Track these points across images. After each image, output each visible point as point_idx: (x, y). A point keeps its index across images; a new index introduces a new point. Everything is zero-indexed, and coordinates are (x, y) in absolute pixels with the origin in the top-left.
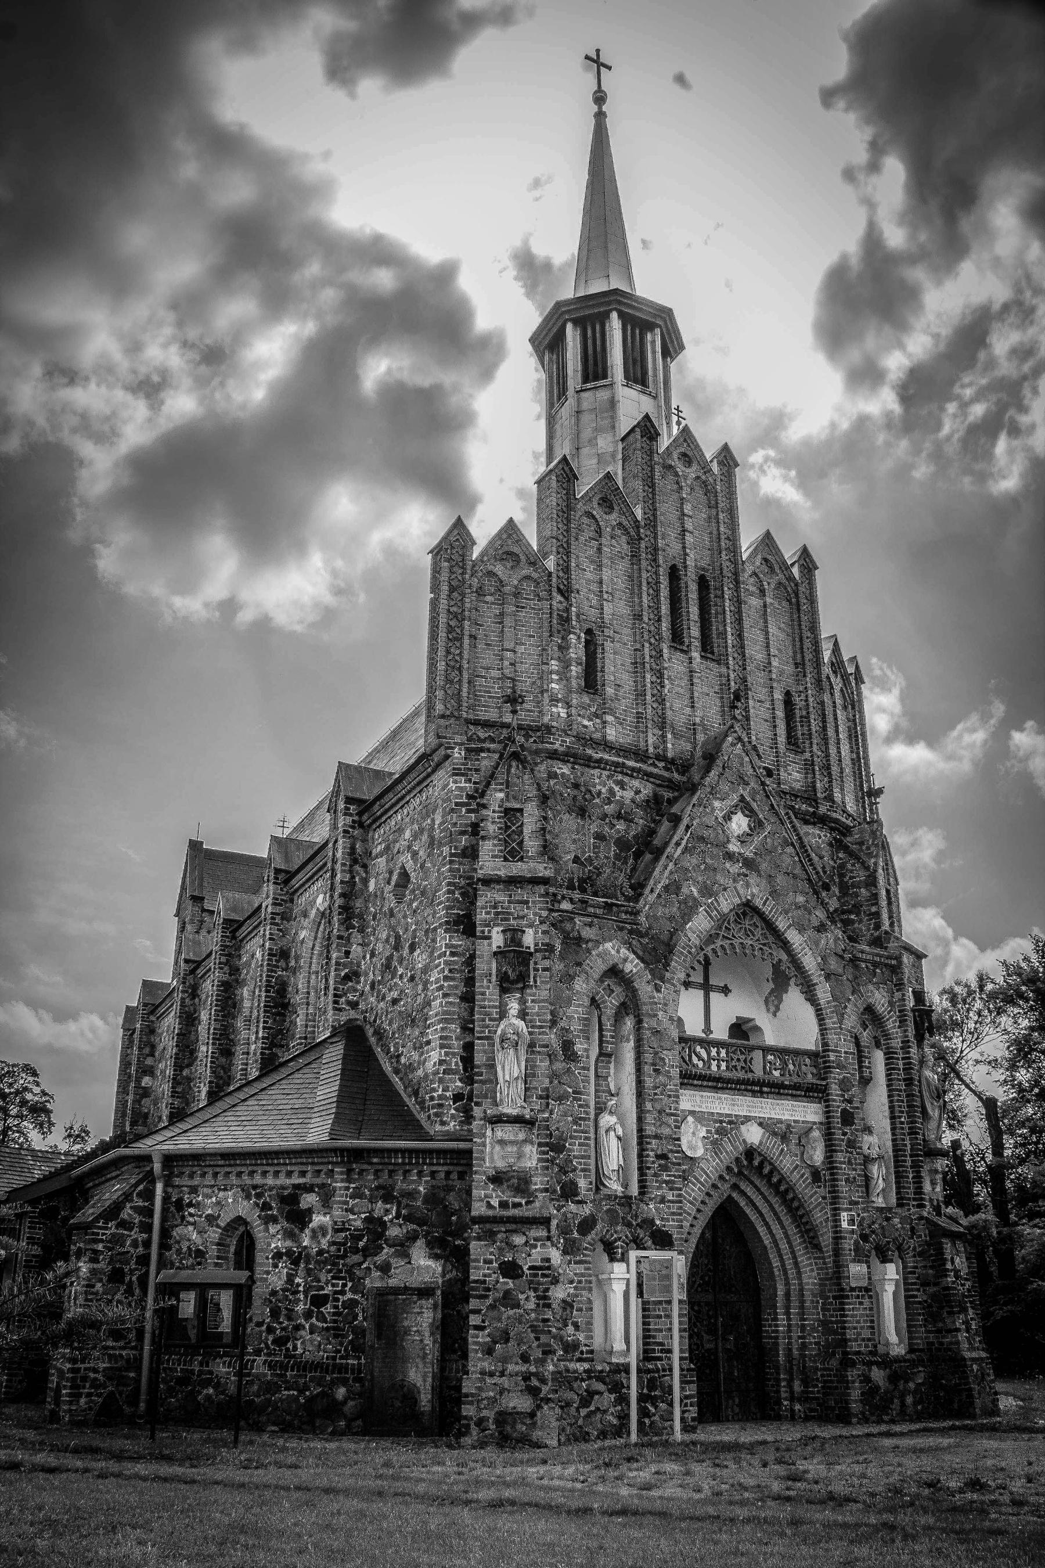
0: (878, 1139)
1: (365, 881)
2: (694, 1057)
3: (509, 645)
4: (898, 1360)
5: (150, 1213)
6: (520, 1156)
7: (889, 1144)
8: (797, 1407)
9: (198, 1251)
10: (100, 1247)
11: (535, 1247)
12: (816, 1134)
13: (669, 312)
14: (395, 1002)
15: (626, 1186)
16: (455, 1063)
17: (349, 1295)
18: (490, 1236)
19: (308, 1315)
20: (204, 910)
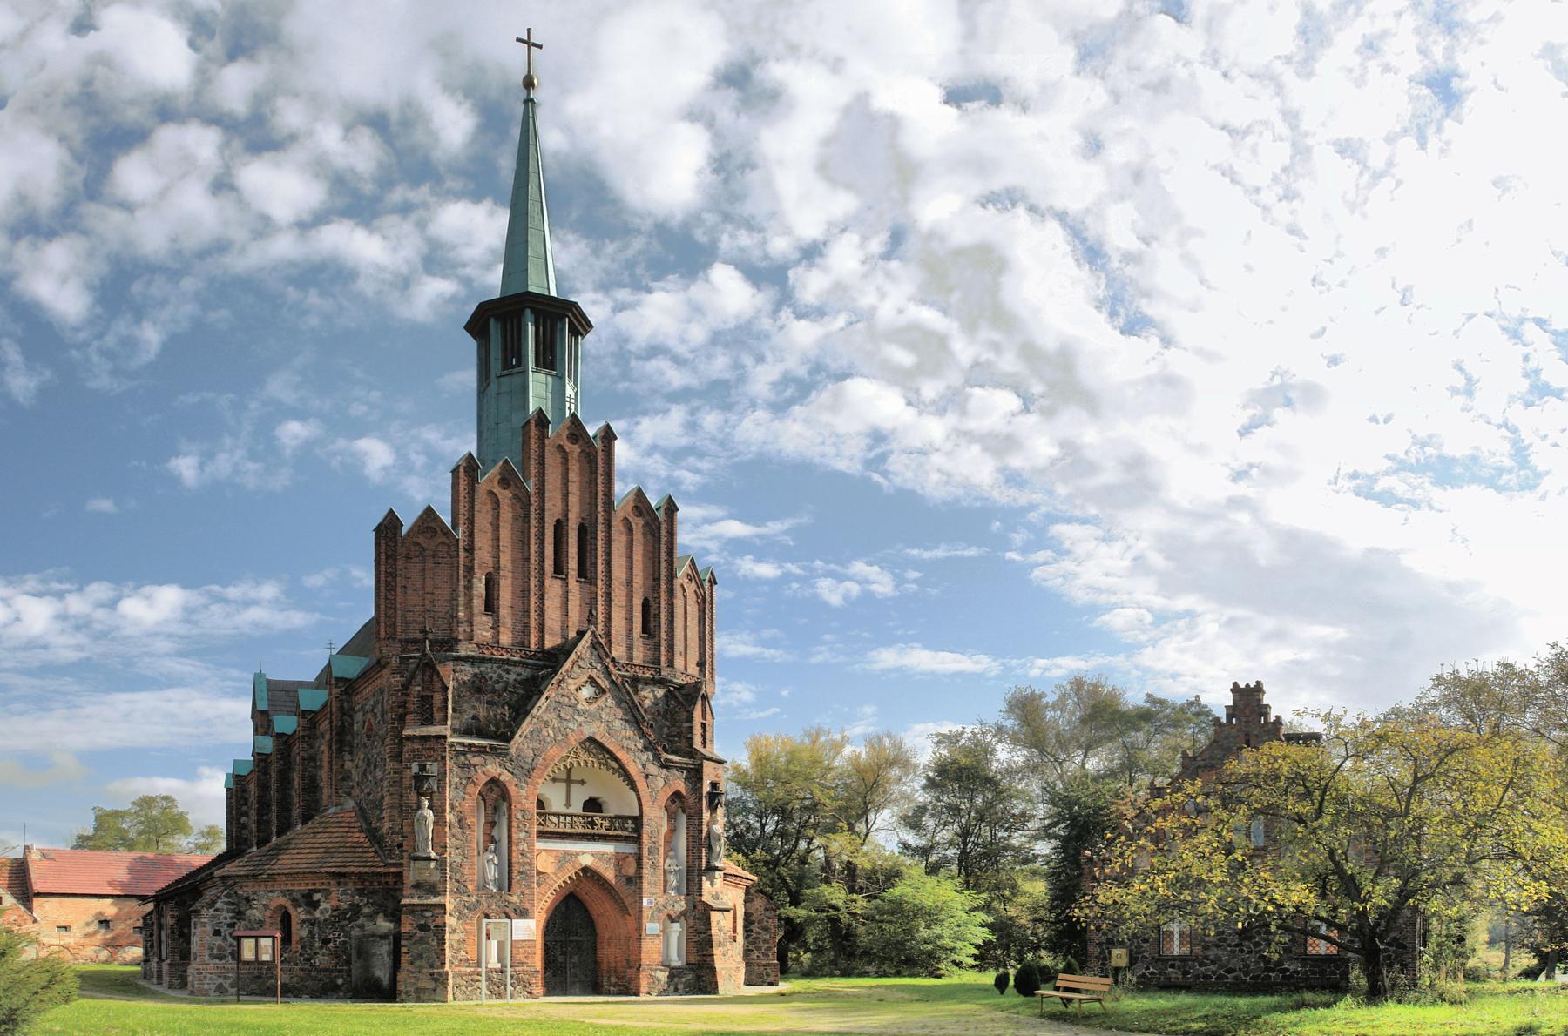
13: (378, 530)
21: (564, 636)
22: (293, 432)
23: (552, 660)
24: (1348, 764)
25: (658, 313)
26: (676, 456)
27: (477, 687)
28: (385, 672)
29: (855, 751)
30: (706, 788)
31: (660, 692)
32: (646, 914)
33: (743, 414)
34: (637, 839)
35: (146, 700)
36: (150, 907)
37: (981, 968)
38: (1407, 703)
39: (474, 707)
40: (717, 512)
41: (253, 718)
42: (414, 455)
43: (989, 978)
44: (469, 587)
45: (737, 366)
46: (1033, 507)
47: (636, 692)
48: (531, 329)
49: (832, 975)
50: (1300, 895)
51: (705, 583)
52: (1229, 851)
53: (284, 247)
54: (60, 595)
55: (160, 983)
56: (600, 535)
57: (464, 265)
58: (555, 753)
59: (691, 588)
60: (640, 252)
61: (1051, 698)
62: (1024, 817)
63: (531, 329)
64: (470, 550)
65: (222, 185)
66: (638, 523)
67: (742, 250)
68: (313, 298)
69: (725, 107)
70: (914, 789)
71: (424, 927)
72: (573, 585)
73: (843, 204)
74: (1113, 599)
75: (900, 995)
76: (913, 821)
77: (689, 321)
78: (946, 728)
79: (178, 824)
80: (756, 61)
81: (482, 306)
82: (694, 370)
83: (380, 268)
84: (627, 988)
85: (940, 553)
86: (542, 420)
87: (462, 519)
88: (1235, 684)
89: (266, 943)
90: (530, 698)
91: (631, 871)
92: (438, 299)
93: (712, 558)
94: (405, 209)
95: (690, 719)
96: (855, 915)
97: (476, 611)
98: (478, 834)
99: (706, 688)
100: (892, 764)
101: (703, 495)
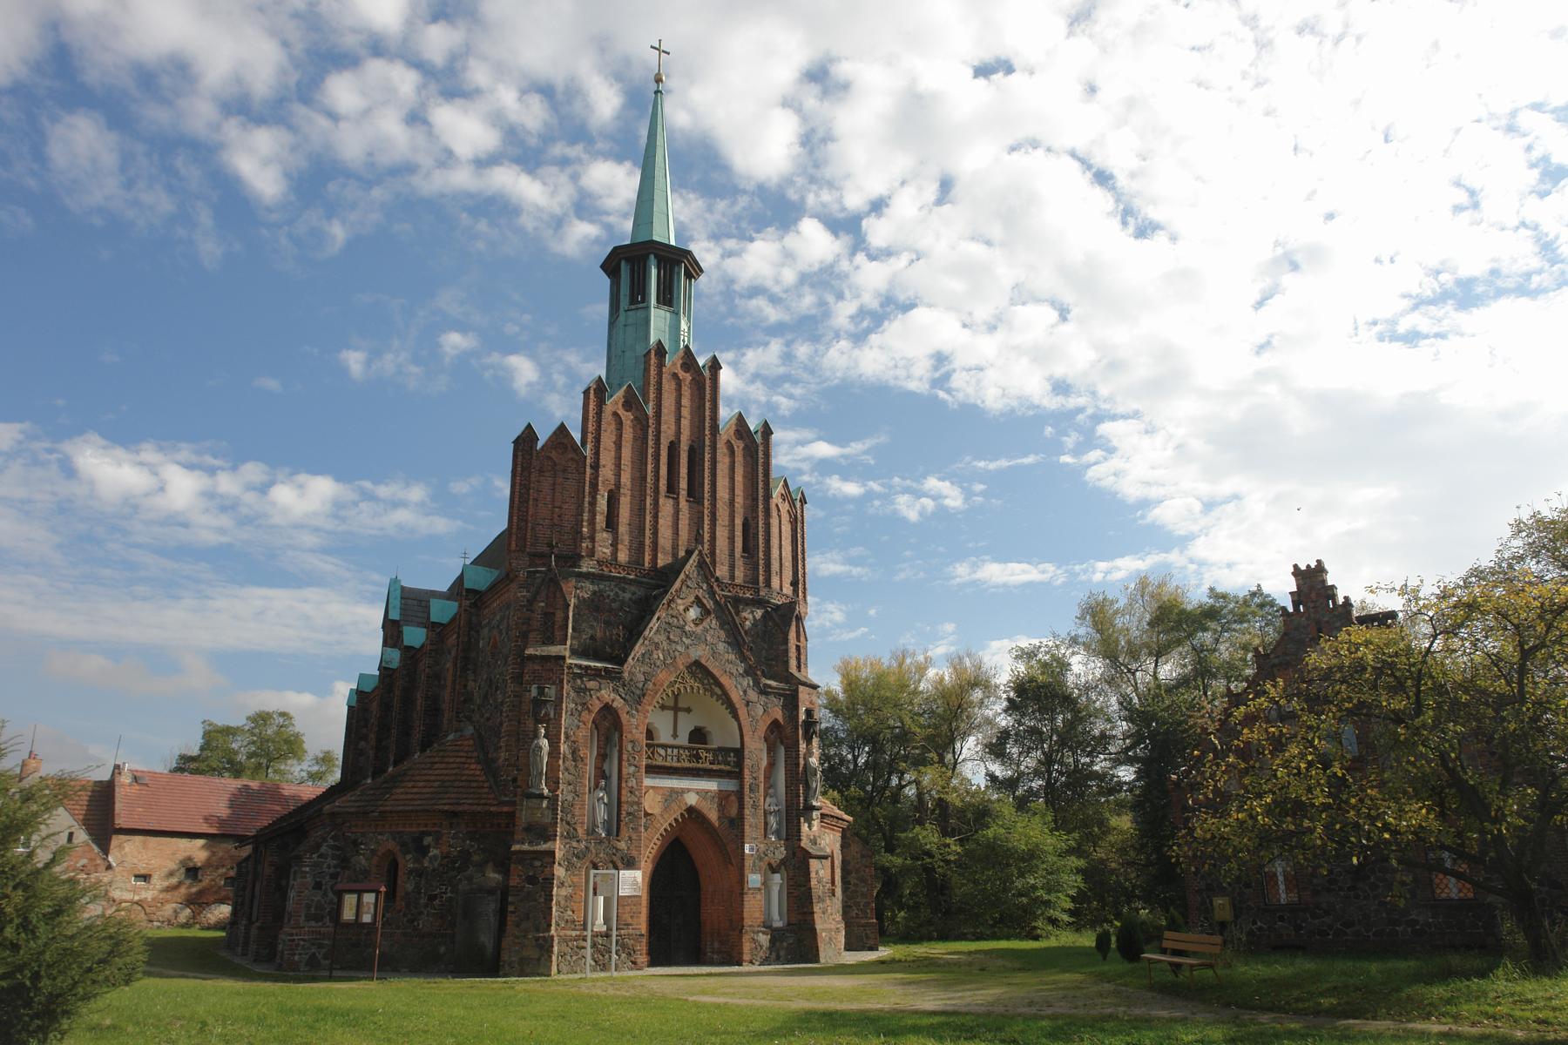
3: (558, 504)
13: (516, 442)
19: (426, 906)
21: (675, 555)
22: (455, 341)
23: (662, 579)
24: (1438, 645)
25: (759, 259)
26: (774, 383)
27: (593, 606)
28: (514, 586)
29: (938, 673)
30: (802, 717)
31: (759, 613)
32: (748, 863)
33: (828, 346)
34: (739, 775)
35: (281, 599)
36: (247, 850)
37: (1077, 927)
38: (1487, 560)
39: (592, 627)
40: (807, 434)
41: (384, 627)
42: (551, 380)
43: (1087, 940)
44: (593, 504)
45: (822, 303)
46: (1080, 410)
47: (738, 613)
48: (654, 272)
49: (930, 939)
50: (1418, 815)
51: (796, 502)
52: (1327, 765)
53: (462, 179)
54: (212, 471)
55: (244, 954)
56: (707, 456)
57: (608, 214)
58: (664, 677)
59: (785, 507)
60: (744, 209)
61: (1122, 603)
62: (1104, 739)
63: (654, 272)
64: (596, 466)
65: (416, 118)
66: (739, 446)
67: (824, 205)
68: (482, 226)
69: (811, 102)
70: (996, 713)
71: (532, 880)
72: (683, 504)
73: (902, 163)
74: (1162, 491)
75: (1000, 962)
76: (996, 749)
77: (783, 265)
78: (1025, 643)
79: (291, 746)
80: (832, 60)
81: (615, 249)
82: (788, 309)
83: (539, 209)
84: (732, 957)
85: (1003, 463)
86: (660, 350)
87: (590, 437)
88: (1296, 566)
89: (369, 898)
90: (642, 618)
91: (734, 812)
92: (584, 239)
93: (806, 478)
94: (564, 162)
95: (786, 641)
96: (947, 862)
97: (598, 527)
98: (589, 768)
99: (800, 609)
100: (974, 684)
101: (797, 420)
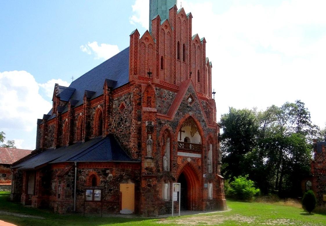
0: (210, 160)
1: (112, 105)
2: (180, 146)
4: (211, 200)
5: (74, 173)
6: (151, 164)
7: (212, 162)
8: (194, 208)
9: (85, 181)
10: (65, 180)
11: (154, 181)
12: (200, 160)
14: (121, 132)
15: (167, 169)
16: (136, 146)
17: (116, 189)
18: (146, 179)
19: (108, 193)
20: (60, 100)
